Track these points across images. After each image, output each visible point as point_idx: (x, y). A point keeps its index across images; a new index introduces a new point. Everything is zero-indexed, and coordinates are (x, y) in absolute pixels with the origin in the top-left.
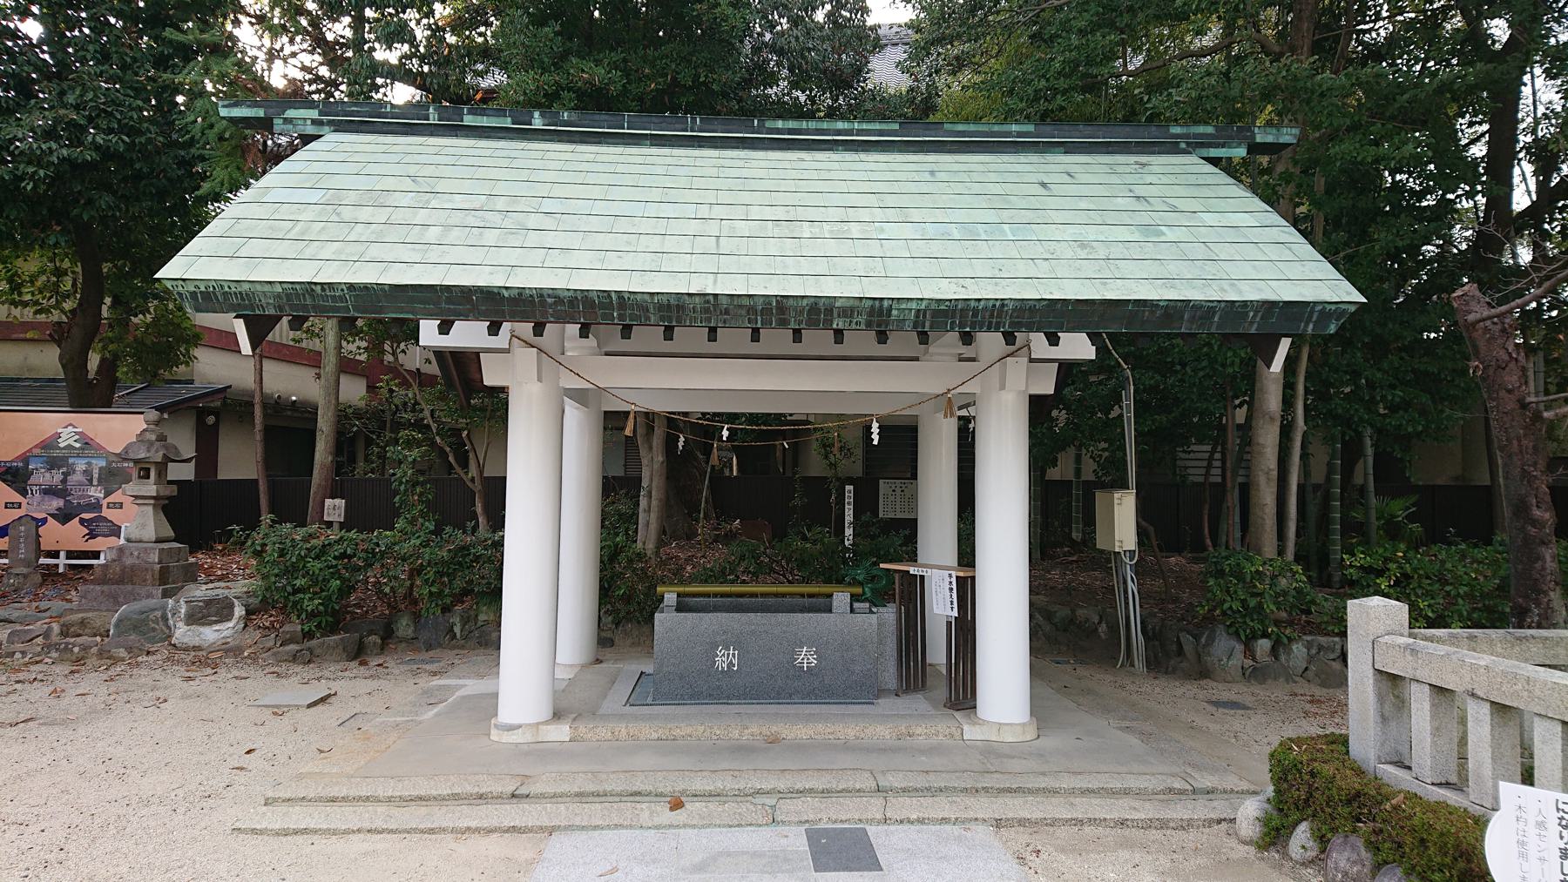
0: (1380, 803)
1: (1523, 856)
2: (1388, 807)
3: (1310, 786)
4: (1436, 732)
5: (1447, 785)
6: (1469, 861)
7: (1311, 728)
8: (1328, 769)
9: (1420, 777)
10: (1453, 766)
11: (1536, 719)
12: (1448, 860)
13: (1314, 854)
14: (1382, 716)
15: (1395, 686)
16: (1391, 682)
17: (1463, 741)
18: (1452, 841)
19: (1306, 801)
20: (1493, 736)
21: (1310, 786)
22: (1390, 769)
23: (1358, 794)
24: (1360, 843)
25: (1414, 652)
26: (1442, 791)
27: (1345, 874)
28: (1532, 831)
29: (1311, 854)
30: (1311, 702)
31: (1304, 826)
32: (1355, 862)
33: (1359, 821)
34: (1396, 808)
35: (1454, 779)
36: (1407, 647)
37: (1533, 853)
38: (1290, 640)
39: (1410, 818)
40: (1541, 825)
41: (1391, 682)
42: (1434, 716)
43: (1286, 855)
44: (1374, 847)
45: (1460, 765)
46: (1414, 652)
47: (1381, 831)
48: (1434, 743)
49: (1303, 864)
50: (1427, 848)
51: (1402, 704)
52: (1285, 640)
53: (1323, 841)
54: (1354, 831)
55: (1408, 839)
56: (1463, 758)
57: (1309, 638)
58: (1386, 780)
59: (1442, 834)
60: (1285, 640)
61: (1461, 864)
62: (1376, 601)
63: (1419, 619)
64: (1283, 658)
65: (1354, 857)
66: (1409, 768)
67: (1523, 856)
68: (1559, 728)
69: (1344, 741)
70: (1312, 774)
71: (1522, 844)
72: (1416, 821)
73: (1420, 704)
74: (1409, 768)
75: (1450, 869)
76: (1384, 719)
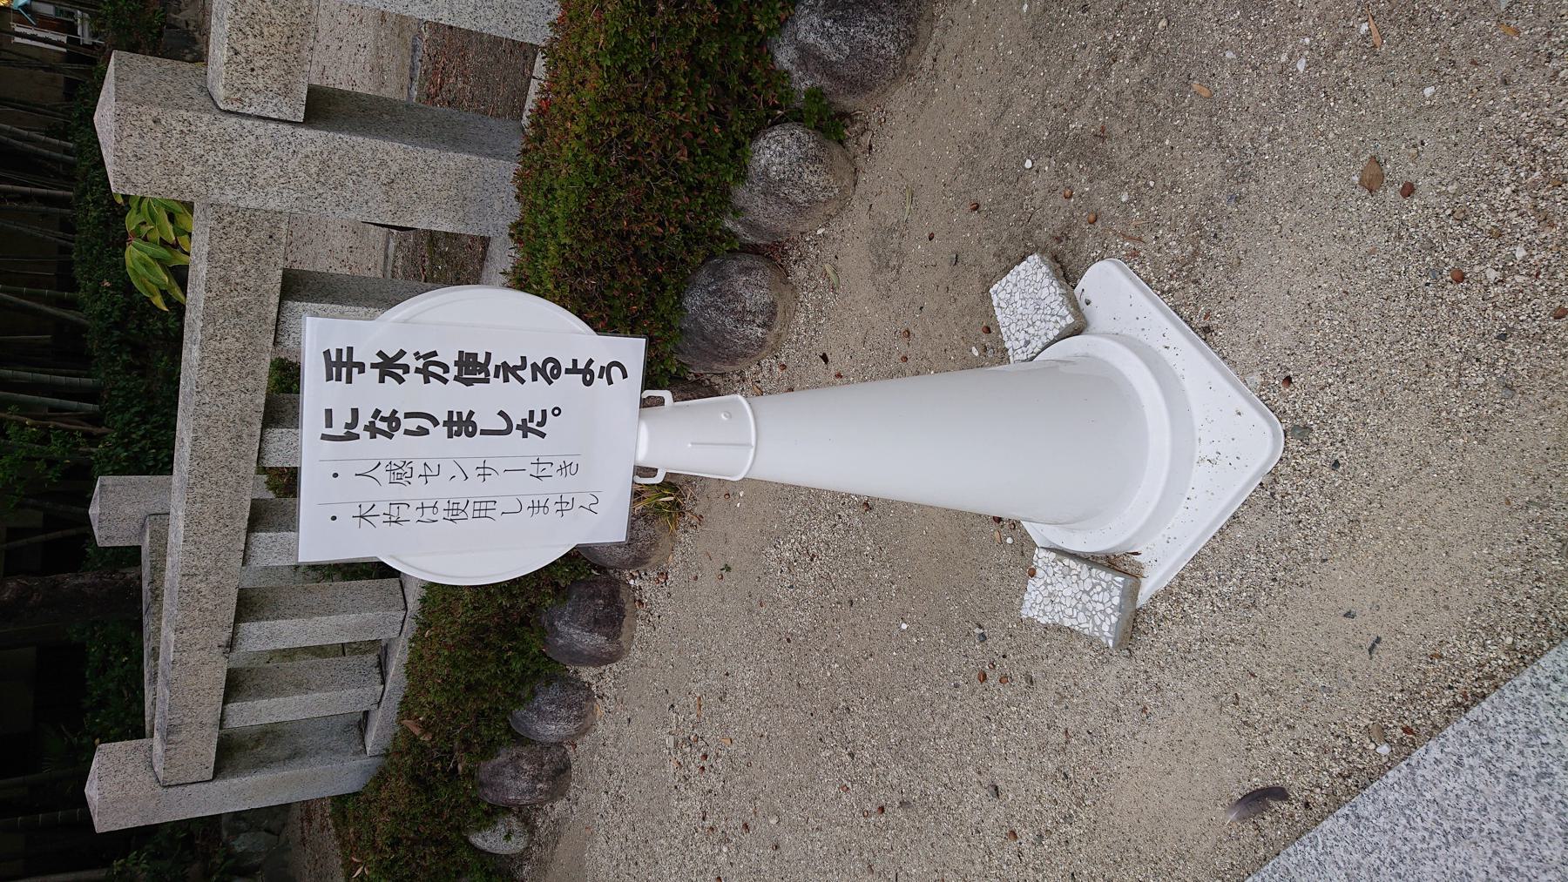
0: (423, 749)
1: (484, 509)
2: (426, 738)
3: (415, 842)
4: (301, 686)
5: (382, 666)
6: (487, 629)
7: (330, 841)
8: (384, 823)
9: (381, 700)
10: (351, 660)
11: (253, 563)
12: (490, 655)
13: (514, 820)
14: (291, 757)
15: (241, 746)
16: (231, 753)
17: (319, 651)
18: (462, 653)
19: (438, 843)
20: (294, 616)
21: (415, 842)
22: (370, 738)
23: (415, 778)
24: (487, 767)
25: (171, 730)
26: (392, 671)
27: (536, 778)
28: (416, 491)
29: (515, 824)
30: (310, 821)
31: (477, 840)
32: (518, 769)
33: (455, 769)
34: (426, 727)
35: (372, 658)
36: (166, 740)
37: (476, 489)
38: (229, 856)
39: (438, 709)
40: (399, 472)
41: (231, 753)
42: (279, 691)
43: (523, 857)
44: (489, 749)
45: (353, 652)
46: (171, 730)
47: (464, 741)
48: (320, 688)
49: (532, 832)
50: (478, 682)
51: (270, 735)
52: (230, 862)
53: (493, 813)
54: (470, 775)
55: (471, 706)
56: (343, 649)
57: (225, 833)
58: (387, 742)
59: (455, 666)
60: (230, 862)
61: (493, 638)
62: (92, 791)
63: (135, 728)
64: (256, 861)
65: (509, 770)
66: (366, 713)
67: (484, 509)
68: (262, 536)
69: (340, 800)
70: (395, 843)
71: (455, 513)
72: (441, 700)
73: (251, 714)
74: (366, 713)
75: (501, 650)
76: (295, 755)
